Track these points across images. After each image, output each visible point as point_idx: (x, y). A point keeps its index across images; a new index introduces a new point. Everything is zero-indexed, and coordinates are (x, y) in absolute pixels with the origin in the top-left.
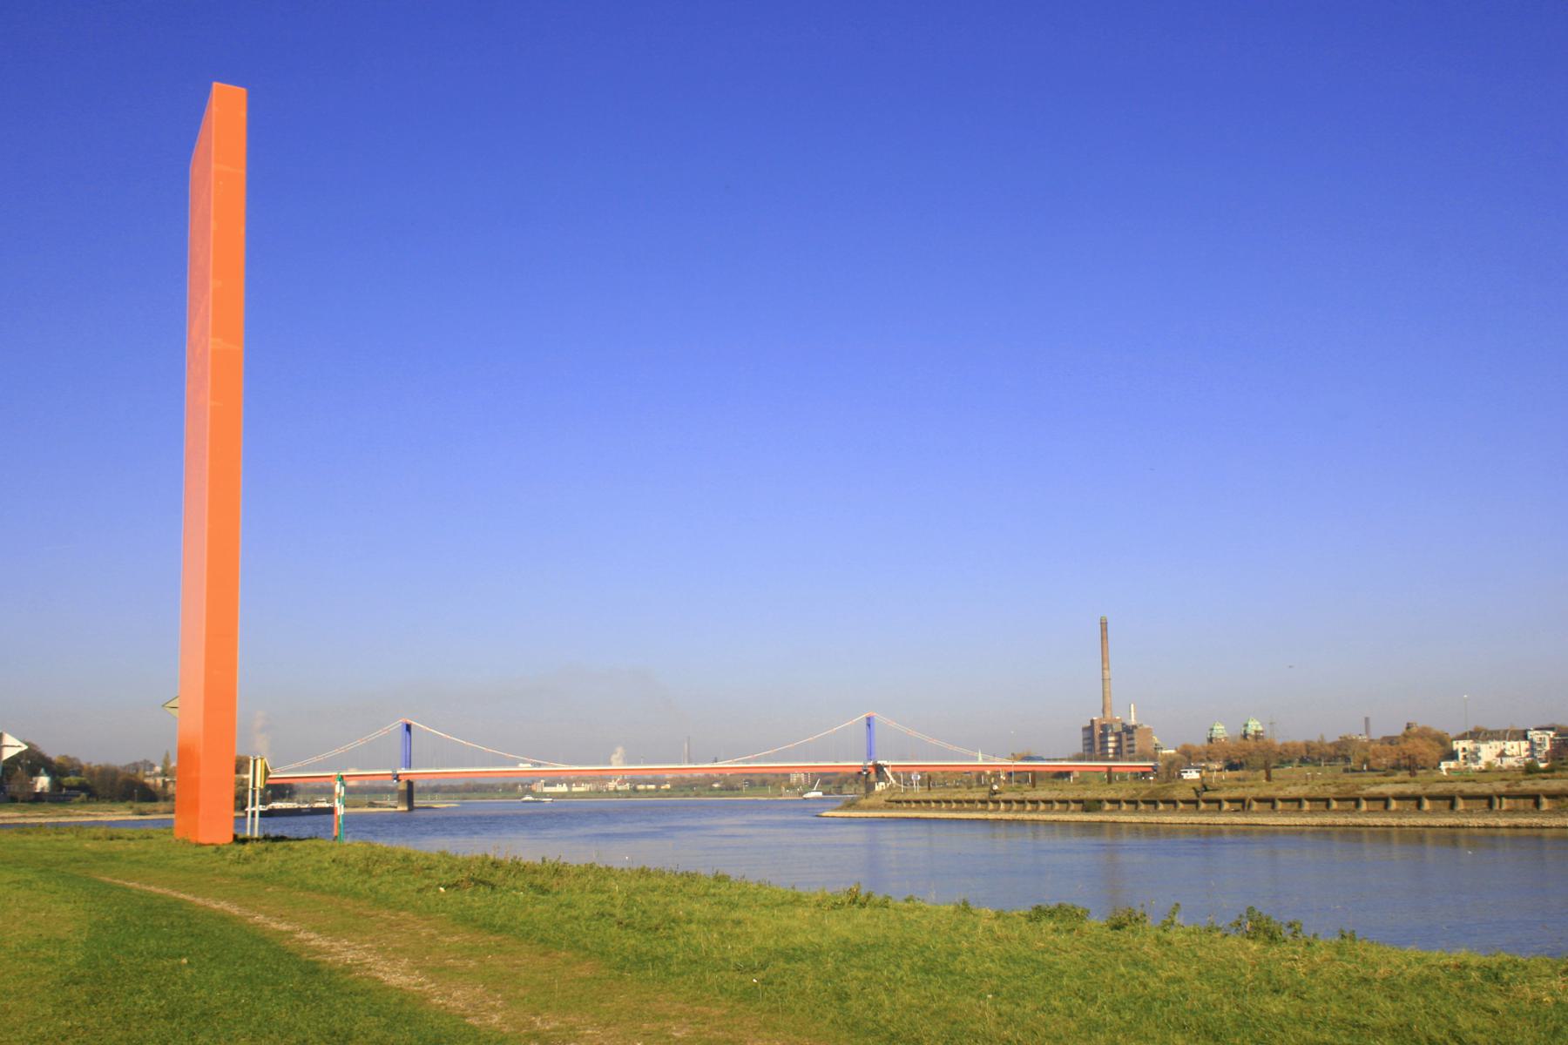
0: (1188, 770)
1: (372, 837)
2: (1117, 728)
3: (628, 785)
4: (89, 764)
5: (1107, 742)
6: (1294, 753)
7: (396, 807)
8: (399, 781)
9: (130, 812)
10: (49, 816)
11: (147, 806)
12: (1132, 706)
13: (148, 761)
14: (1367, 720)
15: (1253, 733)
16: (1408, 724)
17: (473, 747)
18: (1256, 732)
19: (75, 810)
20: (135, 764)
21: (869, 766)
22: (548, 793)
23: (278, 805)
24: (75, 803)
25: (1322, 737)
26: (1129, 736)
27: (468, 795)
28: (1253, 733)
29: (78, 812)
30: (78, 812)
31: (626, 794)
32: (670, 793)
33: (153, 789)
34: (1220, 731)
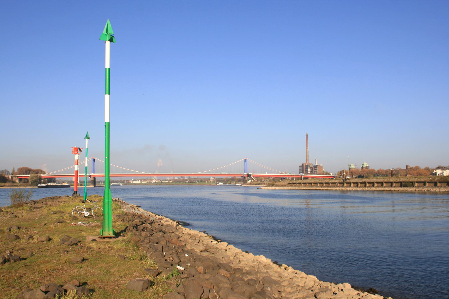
1: (391, 175)
2: (311, 166)
3: (159, 181)
5: (308, 170)
6: (381, 173)
7: (90, 186)
8: (91, 177)
12: (316, 160)
13: (7, 170)
15: (365, 167)
16: (407, 166)
18: (366, 166)
20: (2, 171)
21: (245, 175)
22: (143, 183)
23: (49, 184)
25: (380, 169)
26: (315, 168)
28: (365, 167)
32: (172, 183)
33: (7, 179)
34: (353, 166)
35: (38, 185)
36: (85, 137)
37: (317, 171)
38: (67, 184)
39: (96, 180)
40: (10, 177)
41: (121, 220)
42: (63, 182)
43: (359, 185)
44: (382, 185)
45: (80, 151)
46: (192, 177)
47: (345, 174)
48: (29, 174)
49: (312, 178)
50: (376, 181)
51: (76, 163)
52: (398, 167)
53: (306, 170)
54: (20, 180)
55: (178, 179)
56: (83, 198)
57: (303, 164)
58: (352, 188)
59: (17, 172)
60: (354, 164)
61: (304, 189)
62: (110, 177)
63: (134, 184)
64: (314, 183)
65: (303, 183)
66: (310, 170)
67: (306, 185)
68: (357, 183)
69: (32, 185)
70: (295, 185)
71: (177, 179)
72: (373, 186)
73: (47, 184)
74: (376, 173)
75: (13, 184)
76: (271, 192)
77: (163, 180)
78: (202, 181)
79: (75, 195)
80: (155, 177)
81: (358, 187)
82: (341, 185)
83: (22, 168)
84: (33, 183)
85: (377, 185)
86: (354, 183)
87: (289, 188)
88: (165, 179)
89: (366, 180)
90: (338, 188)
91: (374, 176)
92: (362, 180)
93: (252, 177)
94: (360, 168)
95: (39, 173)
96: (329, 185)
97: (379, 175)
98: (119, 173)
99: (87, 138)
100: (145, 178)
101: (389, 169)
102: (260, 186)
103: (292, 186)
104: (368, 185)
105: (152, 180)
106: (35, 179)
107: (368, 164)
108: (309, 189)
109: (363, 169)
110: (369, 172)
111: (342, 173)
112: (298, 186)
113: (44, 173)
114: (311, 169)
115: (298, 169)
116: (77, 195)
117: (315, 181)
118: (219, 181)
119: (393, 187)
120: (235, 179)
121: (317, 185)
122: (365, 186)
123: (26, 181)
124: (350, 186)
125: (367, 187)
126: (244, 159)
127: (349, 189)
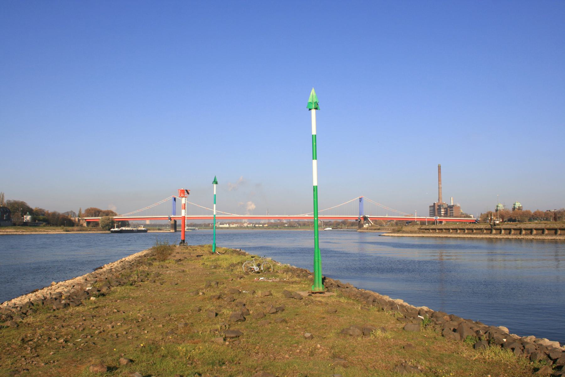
2: (445, 206)
3: (251, 224)
4: (48, 211)
5: (441, 211)
6: (539, 215)
7: (170, 231)
8: (171, 220)
9: (62, 231)
10: (27, 232)
11: (70, 228)
15: (518, 208)
18: (519, 207)
19: (39, 229)
20: (68, 212)
21: (361, 217)
23: (124, 228)
24: (41, 226)
25: (538, 210)
26: (451, 209)
29: (40, 230)
30: (40, 230)
32: (268, 228)
33: (74, 222)
34: (501, 207)
35: (111, 230)
36: (213, 182)
37: (453, 213)
38: (144, 229)
39: (177, 224)
40: (77, 219)
41: (297, 276)
42: (139, 225)
43: (513, 232)
44: (543, 233)
45: (188, 193)
46: (292, 220)
47: (493, 218)
48: (98, 216)
49: (447, 221)
50: (534, 227)
51: (183, 208)
52: (562, 208)
53: (439, 211)
54: (88, 223)
55: (274, 222)
56: (212, 249)
57: (434, 204)
58: (503, 236)
59: (85, 214)
60: (502, 204)
61: (440, 237)
62: (319, 240)
63: (222, 228)
64: (452, 229)
65: (438, 229)
66: (444, 211)
67: (442, 232)
68: (510, 229)
70: (428, 231)
71: (273, 222)
72: (531, 233)
73: (121, 229)
74: (533, 216)
75: (81, 228)
76: (396, 241)
77: (257, 224)
78: (305, 225)
79: (182, 244)
80: (246, 220)
81: (511, 235)
82: (488, 232)
84: (105, 227)
85: (537, 233)
86: (505, 229)
87: (421, 235)
88: (258, 222)
89: (521, 225)
90: (484, 236)
91: (530, 220)
92: (516, 226)
93: (370, 221)
94: (510, 208)
95: (110, 214)
96: (472, 231)
97: (536, 218)
98: (205, 214)
99: (215, 183)
100: (234, 221)
101: (549, 211)
102: (380, 231)
103: (423, 232)
104: (524, 232)
105: (243, 224)
106: (107, 222)
107: (521, 204)
108: (447, 237)
109: (515, 211)
110: (523, 214)
111: (489, 216)
112: (431, 233)
113: (116, 215)
114: (446, 210)
115: (428, 210)
116: (185, 244)
117: (454, 227)
118: (327, 224)
119: (557, 235)
120: (347, 222)
121: (457, 231)
122: (520, 234)
123: (96, 224)
124: (500, 233)
125: (523, 234)
126: (359, 197)
127: (498, 236)
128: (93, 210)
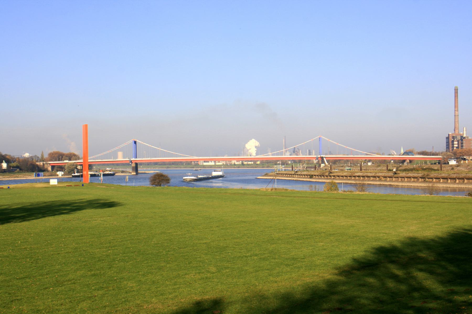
0: (451, 160)
7: (131, 173)
10: (12, 178)
12: (465, 128)
14: (433, 147)
17: (161, 150)
19: (19, 175)
21: (319, 157)
24: (16, 172)
27: (169, 166)
30: (20, 176)
31: (238, 166)
63: (204, 166)
69: (69, 174)
83: (53, 152)
106: (72, 167)
128: (56, 154)
